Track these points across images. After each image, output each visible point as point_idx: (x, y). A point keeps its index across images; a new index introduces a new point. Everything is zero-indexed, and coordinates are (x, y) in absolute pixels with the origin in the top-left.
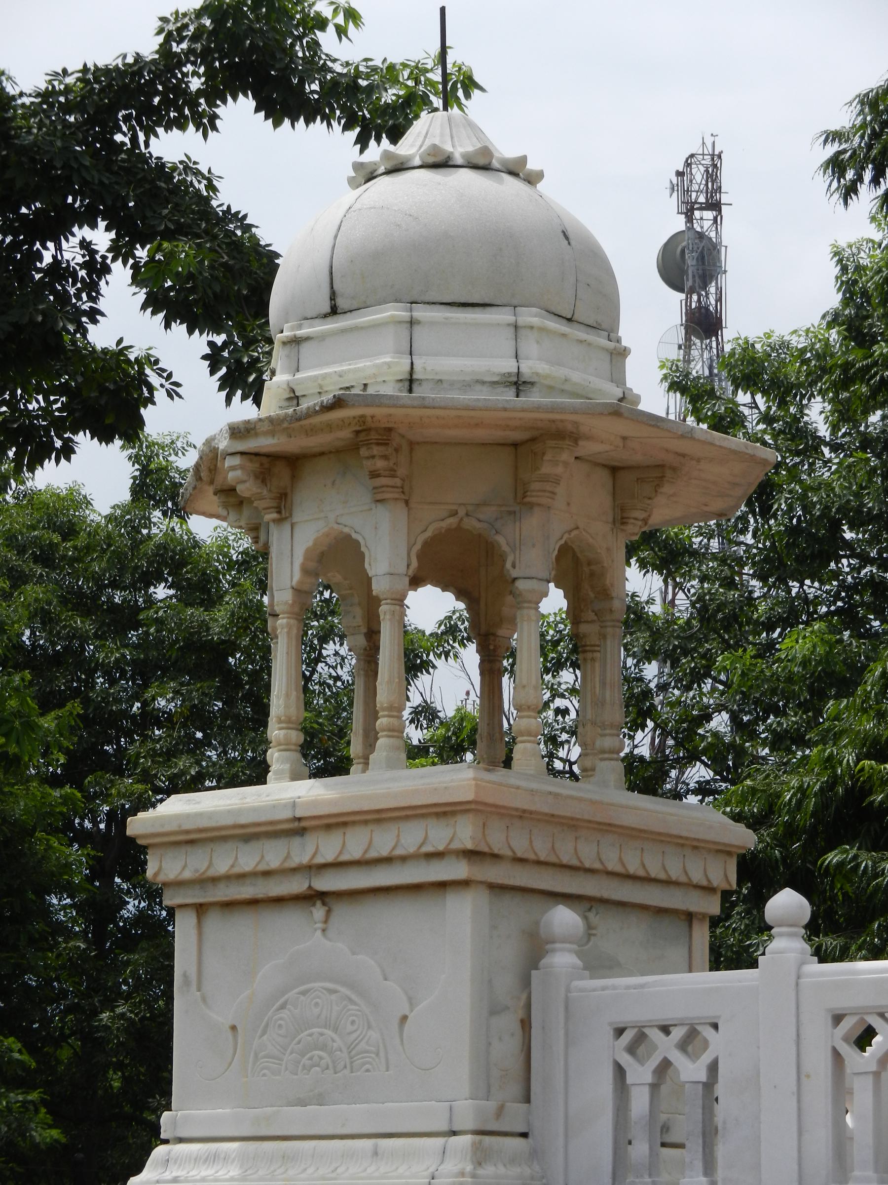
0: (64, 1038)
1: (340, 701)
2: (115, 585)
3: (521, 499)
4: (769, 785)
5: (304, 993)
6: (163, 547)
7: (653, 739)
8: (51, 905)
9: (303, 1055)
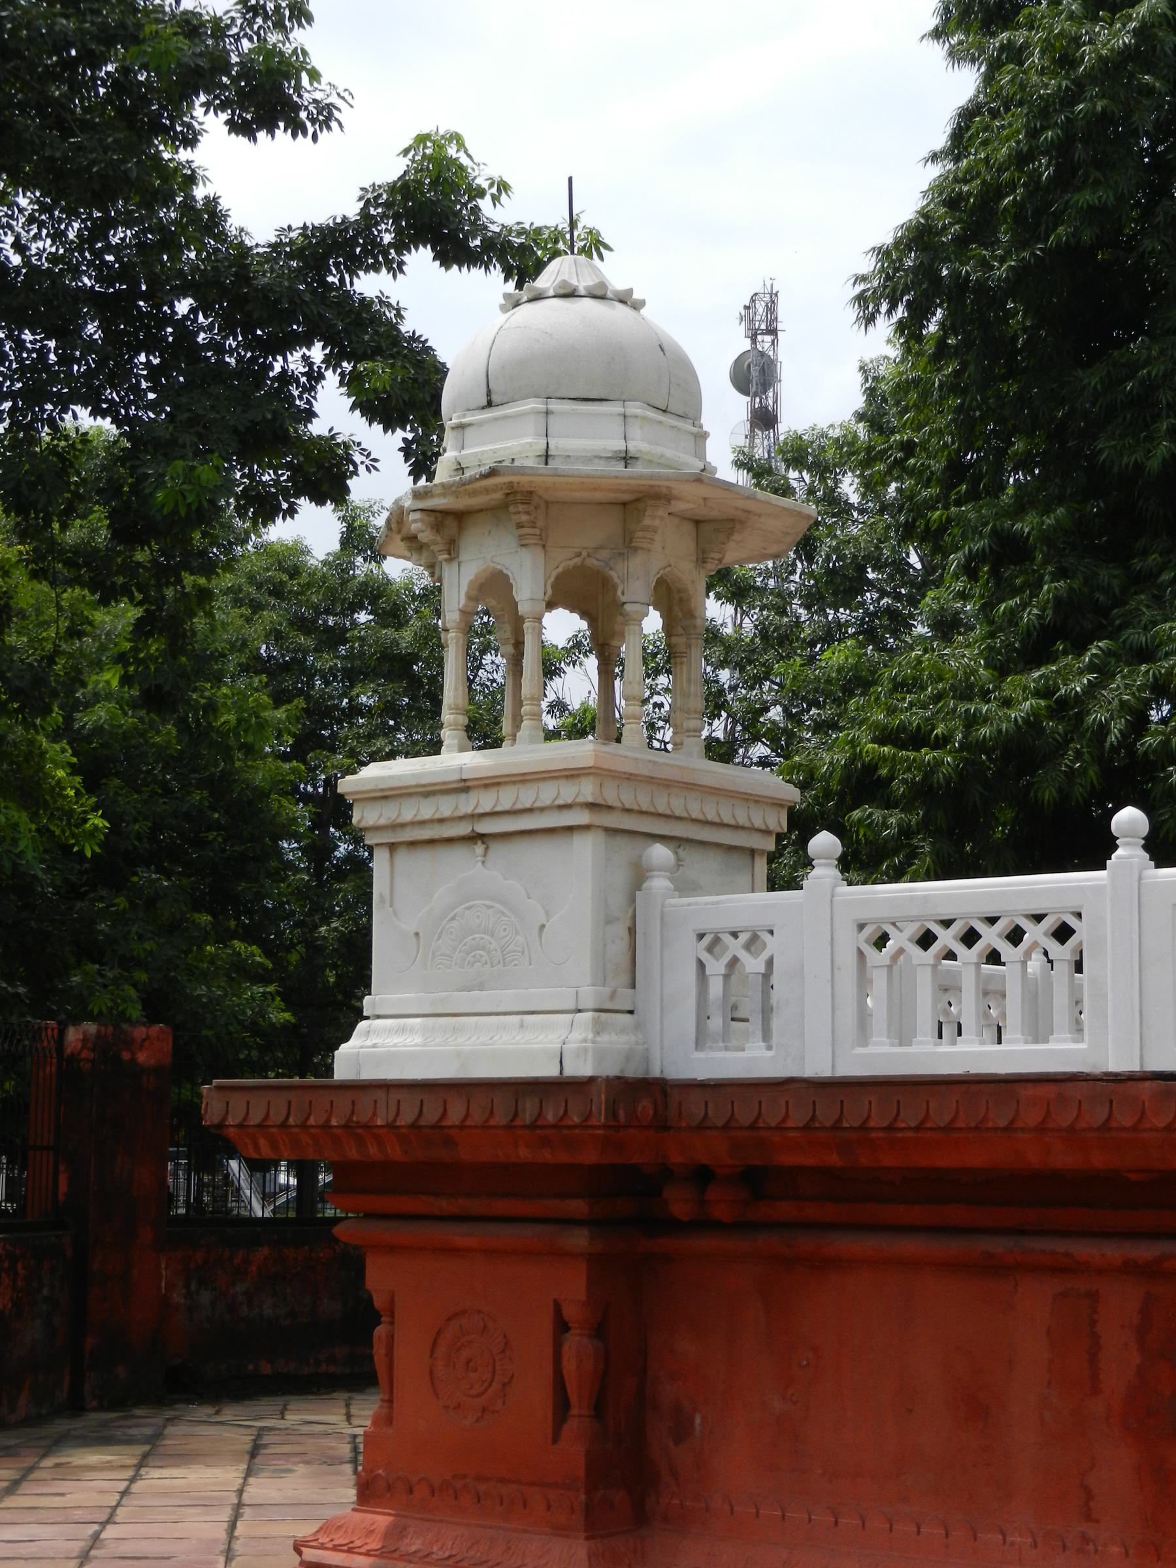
0: (293, 946)
1: (495, 697)
2: (328, 612)
3: (628, 544)
4: (811, 760)
5: (469, 908)
6: (364, 584)
7: (726, 726)
8: (283, 848)
9: (468, 954)
